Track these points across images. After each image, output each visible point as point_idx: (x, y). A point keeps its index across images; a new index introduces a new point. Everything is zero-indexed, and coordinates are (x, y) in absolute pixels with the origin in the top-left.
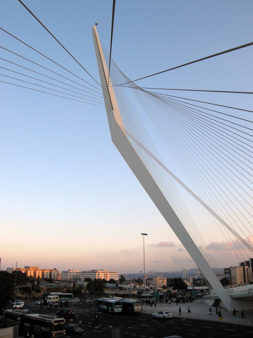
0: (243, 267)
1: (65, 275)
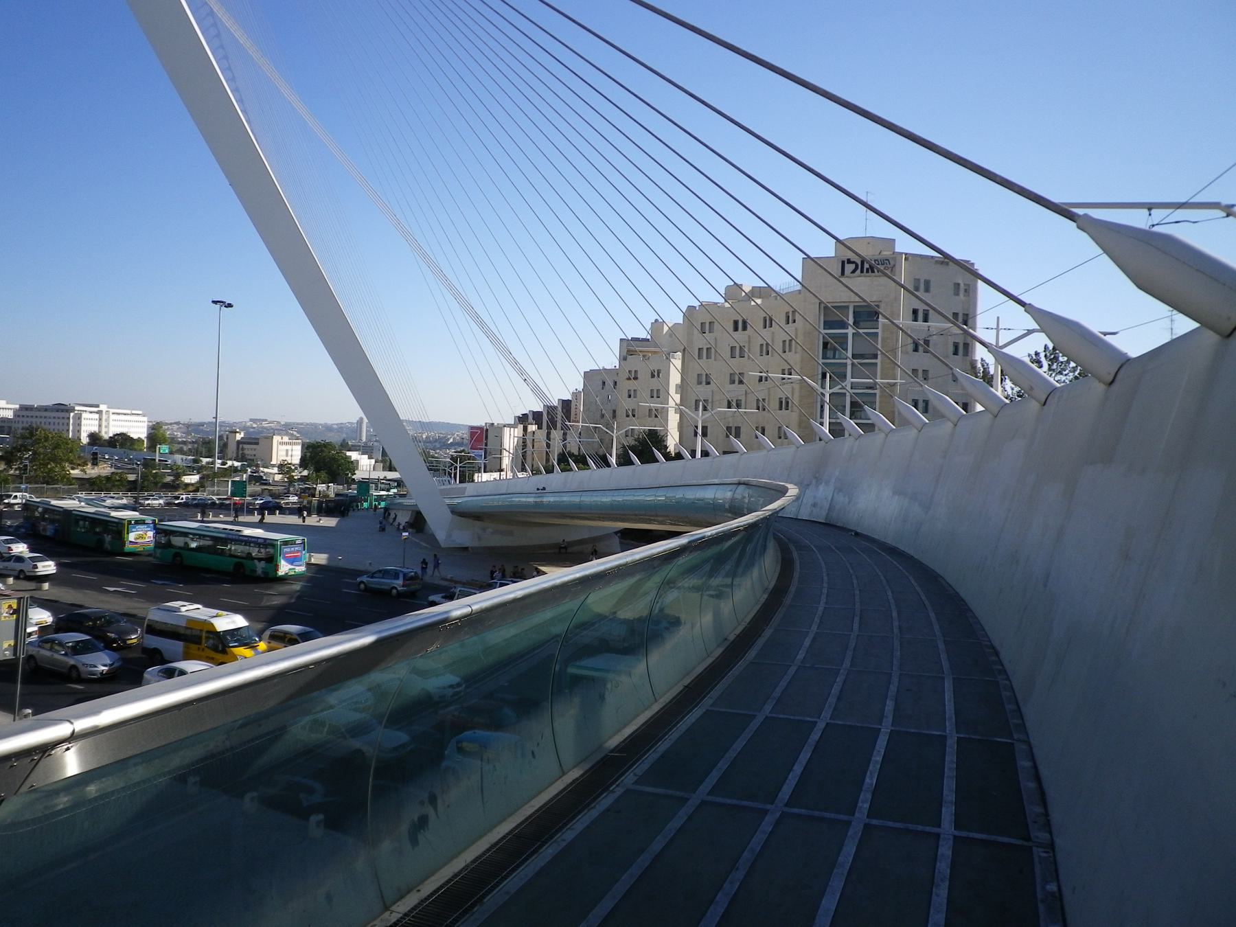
1: (57, 421)
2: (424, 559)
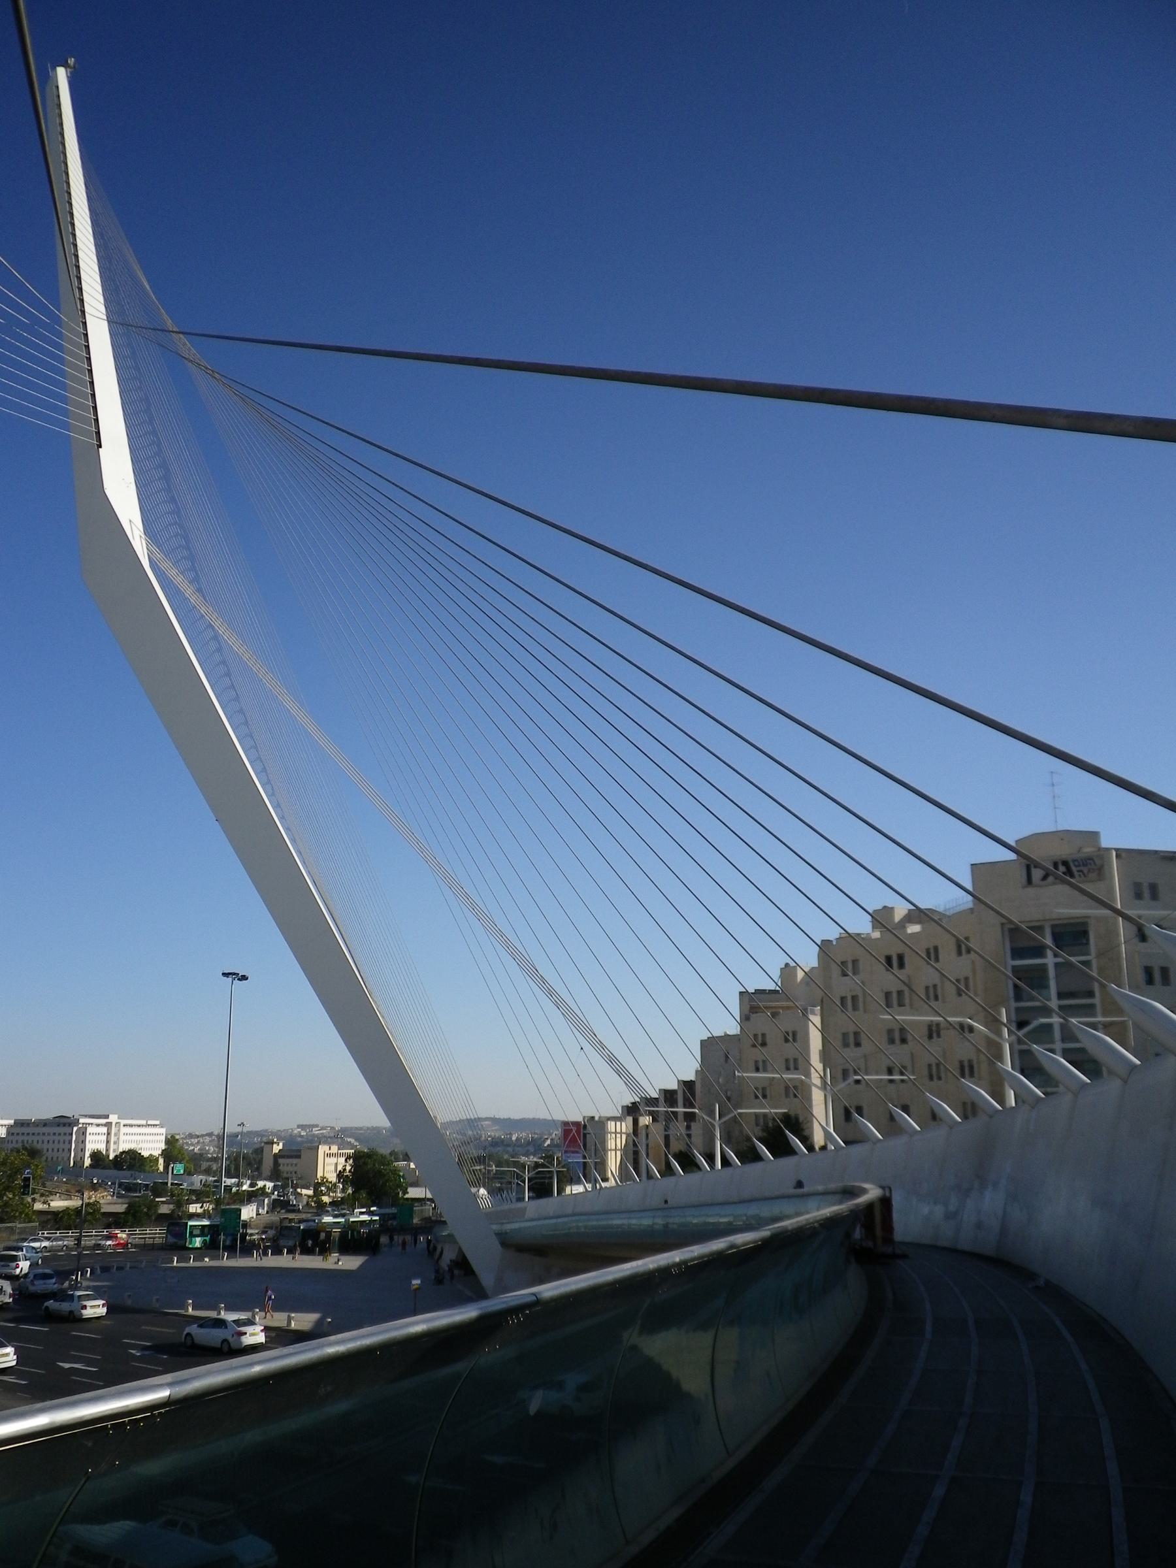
0: (633, 1119)
1: (56, 1138)
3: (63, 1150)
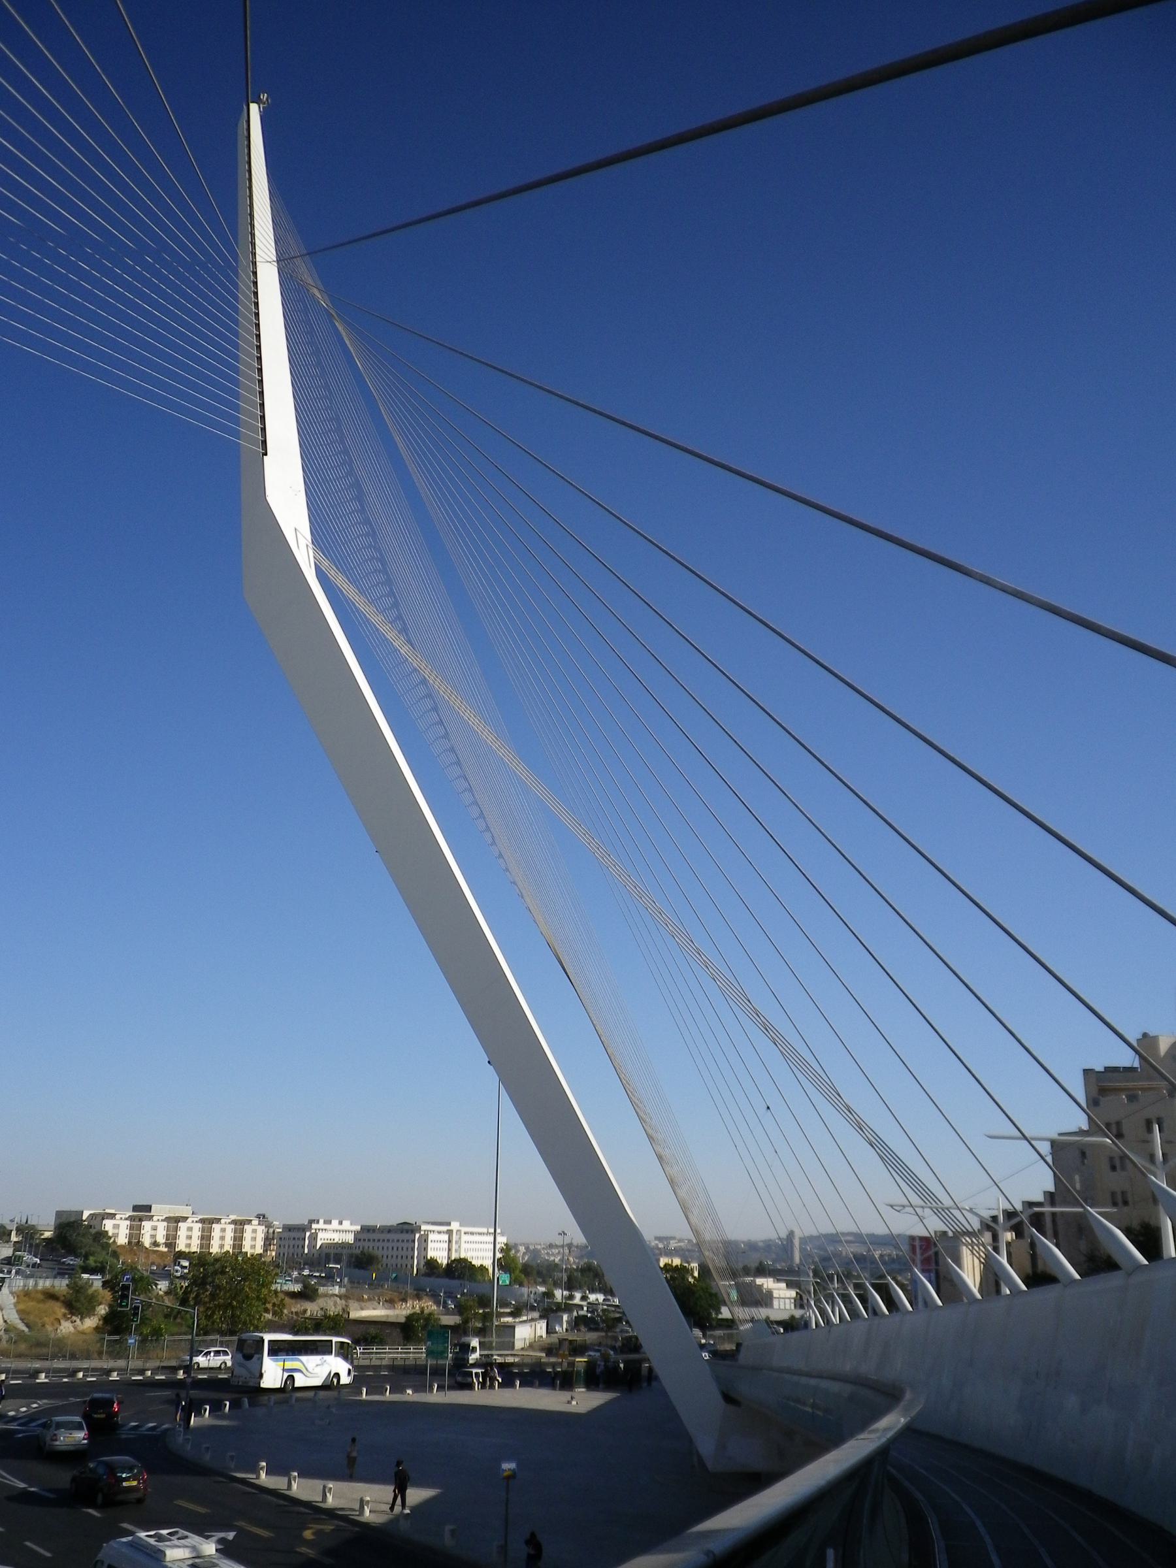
1: (400, 1245)
2: (533, 1535)
3: (392, 1256)
